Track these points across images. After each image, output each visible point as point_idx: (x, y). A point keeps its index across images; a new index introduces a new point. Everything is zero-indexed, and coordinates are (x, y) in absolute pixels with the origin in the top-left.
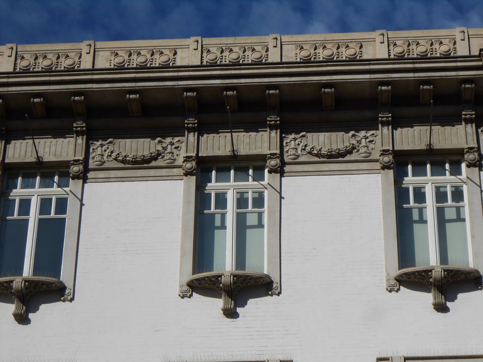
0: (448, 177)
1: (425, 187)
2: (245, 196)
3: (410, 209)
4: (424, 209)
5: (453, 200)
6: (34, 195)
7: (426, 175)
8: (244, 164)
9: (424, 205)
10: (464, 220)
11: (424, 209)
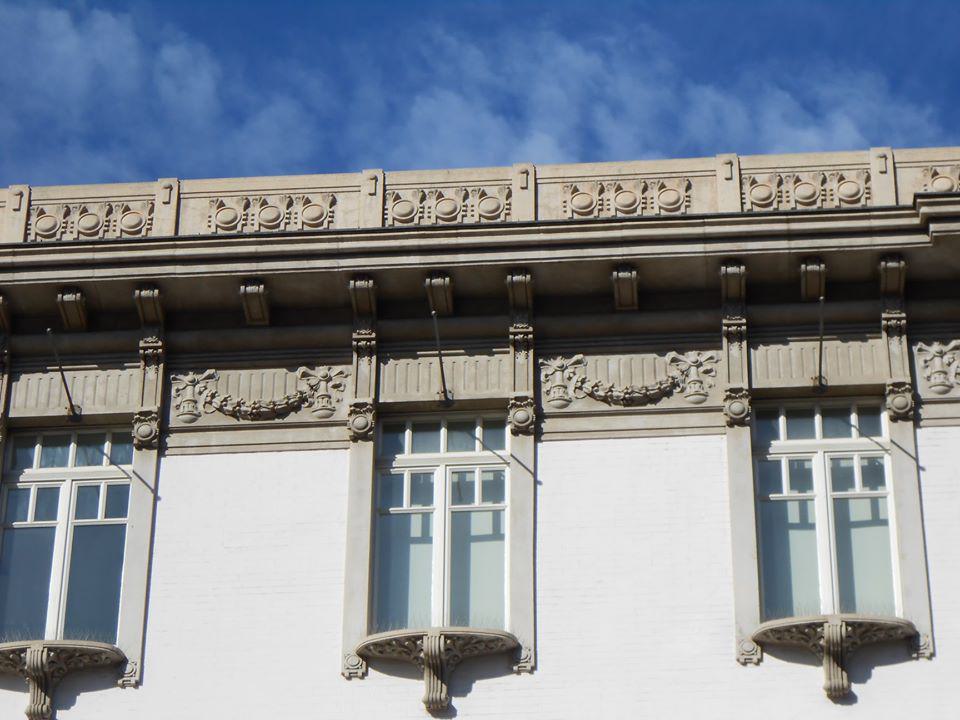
0: (478, 452)
7: (437, 450)
8: (840, 403)
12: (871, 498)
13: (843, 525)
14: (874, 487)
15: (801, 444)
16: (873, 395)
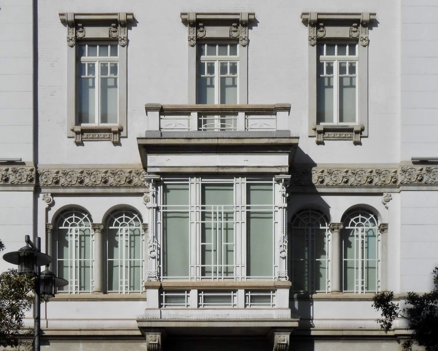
0: (347, 56)
1: (333, 63)
2: (353, 65)
3: (324, 78)
4: (235, 78)
5: (231, 72)
6: (335, 60)
7: (227, 54)
8: (332, 43)
9: (331, 75)
10: (354, 87)
11: (235, 78)
12: (210, 77)
13: (342, 87)
14: (351, 74)
15: (92, 58)
16: (334, 40)
